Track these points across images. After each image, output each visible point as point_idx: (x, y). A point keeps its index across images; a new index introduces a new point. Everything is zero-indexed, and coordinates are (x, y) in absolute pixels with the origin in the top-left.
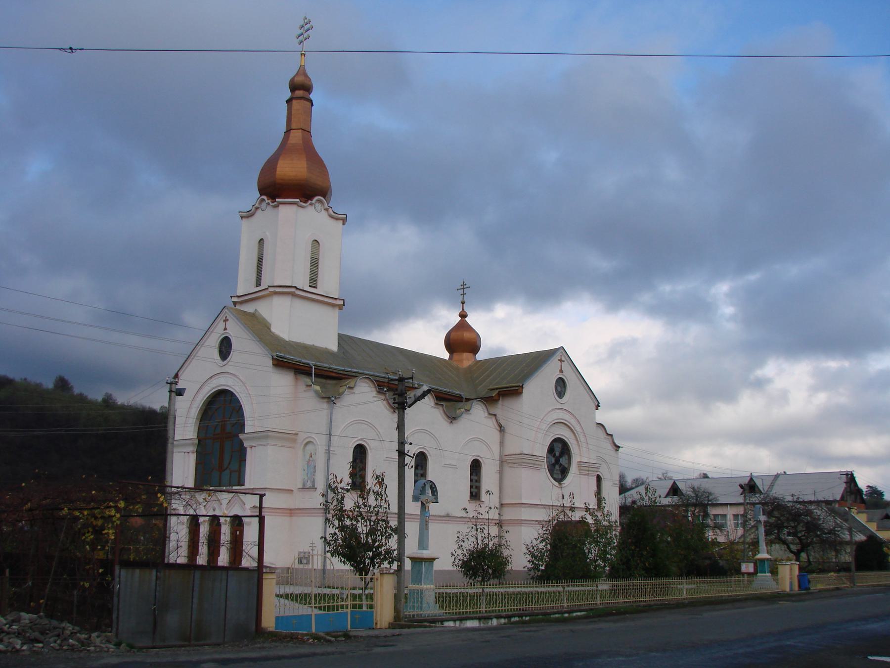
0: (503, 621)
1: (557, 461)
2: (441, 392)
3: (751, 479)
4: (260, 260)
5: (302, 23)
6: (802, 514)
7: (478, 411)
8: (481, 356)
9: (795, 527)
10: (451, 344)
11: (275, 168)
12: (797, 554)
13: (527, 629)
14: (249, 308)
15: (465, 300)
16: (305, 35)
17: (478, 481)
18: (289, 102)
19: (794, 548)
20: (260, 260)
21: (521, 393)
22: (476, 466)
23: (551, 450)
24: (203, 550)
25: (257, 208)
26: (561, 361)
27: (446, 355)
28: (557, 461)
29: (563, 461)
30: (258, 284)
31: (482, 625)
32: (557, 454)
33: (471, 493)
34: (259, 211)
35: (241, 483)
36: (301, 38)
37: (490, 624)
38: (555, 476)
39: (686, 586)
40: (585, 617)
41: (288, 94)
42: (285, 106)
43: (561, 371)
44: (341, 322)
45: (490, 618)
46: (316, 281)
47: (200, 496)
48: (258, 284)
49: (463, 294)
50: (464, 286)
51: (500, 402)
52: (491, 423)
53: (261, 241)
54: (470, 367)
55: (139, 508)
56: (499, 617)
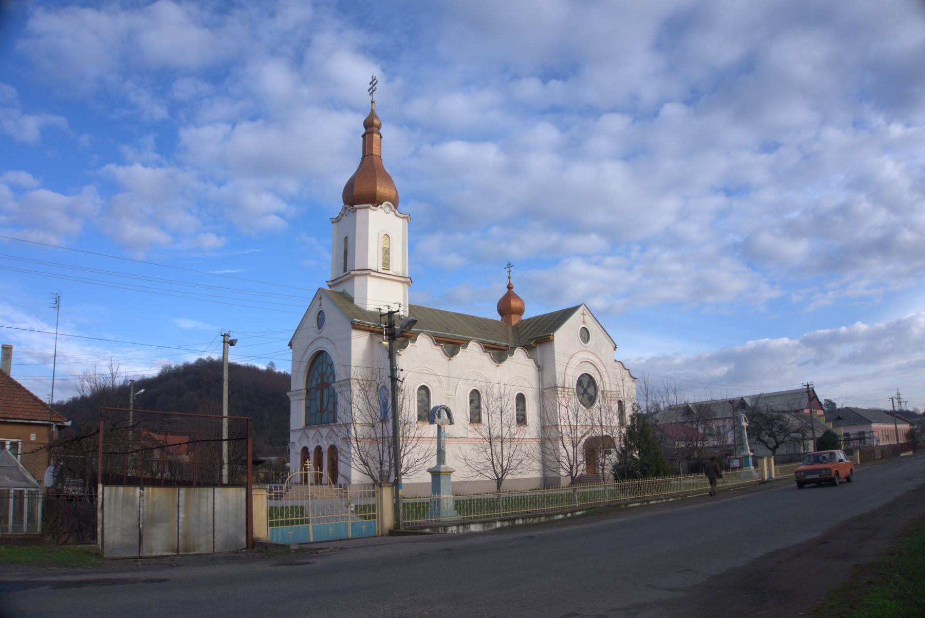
0: (506, 524)
1: (585, 391)
2: (487, 343)
4: (346, 252)
6: (774, 420)
7: (519, 354)
8: (525, 317)
9: (771, 430)
12: (773, 450)
15: (505, 273)
17: (524, 409)
18: (364, 136)
19: (771, 446)
20: (346, 252)
21: (553, 340)
22: (521, 398)
23: (579, 383)
24: (113, 493)
26: (583, 314)
28: (585, 391)
29: (591, 391)
30: (345, 270)
31: (486, 529)
33: (518, 420)
35: (335, 421)
37: (494, 527)
39: (683, 482)
41: (363, 131)
42: (362, 139)
43: (584, 322)
45: (541, 516)
47: (311, 433)
48: (345, 270)
50: (509, 265)
52: (531, 363)
53: (346, 237)
54: (516, 325)
55: (157, 454)
56: (502, 520)
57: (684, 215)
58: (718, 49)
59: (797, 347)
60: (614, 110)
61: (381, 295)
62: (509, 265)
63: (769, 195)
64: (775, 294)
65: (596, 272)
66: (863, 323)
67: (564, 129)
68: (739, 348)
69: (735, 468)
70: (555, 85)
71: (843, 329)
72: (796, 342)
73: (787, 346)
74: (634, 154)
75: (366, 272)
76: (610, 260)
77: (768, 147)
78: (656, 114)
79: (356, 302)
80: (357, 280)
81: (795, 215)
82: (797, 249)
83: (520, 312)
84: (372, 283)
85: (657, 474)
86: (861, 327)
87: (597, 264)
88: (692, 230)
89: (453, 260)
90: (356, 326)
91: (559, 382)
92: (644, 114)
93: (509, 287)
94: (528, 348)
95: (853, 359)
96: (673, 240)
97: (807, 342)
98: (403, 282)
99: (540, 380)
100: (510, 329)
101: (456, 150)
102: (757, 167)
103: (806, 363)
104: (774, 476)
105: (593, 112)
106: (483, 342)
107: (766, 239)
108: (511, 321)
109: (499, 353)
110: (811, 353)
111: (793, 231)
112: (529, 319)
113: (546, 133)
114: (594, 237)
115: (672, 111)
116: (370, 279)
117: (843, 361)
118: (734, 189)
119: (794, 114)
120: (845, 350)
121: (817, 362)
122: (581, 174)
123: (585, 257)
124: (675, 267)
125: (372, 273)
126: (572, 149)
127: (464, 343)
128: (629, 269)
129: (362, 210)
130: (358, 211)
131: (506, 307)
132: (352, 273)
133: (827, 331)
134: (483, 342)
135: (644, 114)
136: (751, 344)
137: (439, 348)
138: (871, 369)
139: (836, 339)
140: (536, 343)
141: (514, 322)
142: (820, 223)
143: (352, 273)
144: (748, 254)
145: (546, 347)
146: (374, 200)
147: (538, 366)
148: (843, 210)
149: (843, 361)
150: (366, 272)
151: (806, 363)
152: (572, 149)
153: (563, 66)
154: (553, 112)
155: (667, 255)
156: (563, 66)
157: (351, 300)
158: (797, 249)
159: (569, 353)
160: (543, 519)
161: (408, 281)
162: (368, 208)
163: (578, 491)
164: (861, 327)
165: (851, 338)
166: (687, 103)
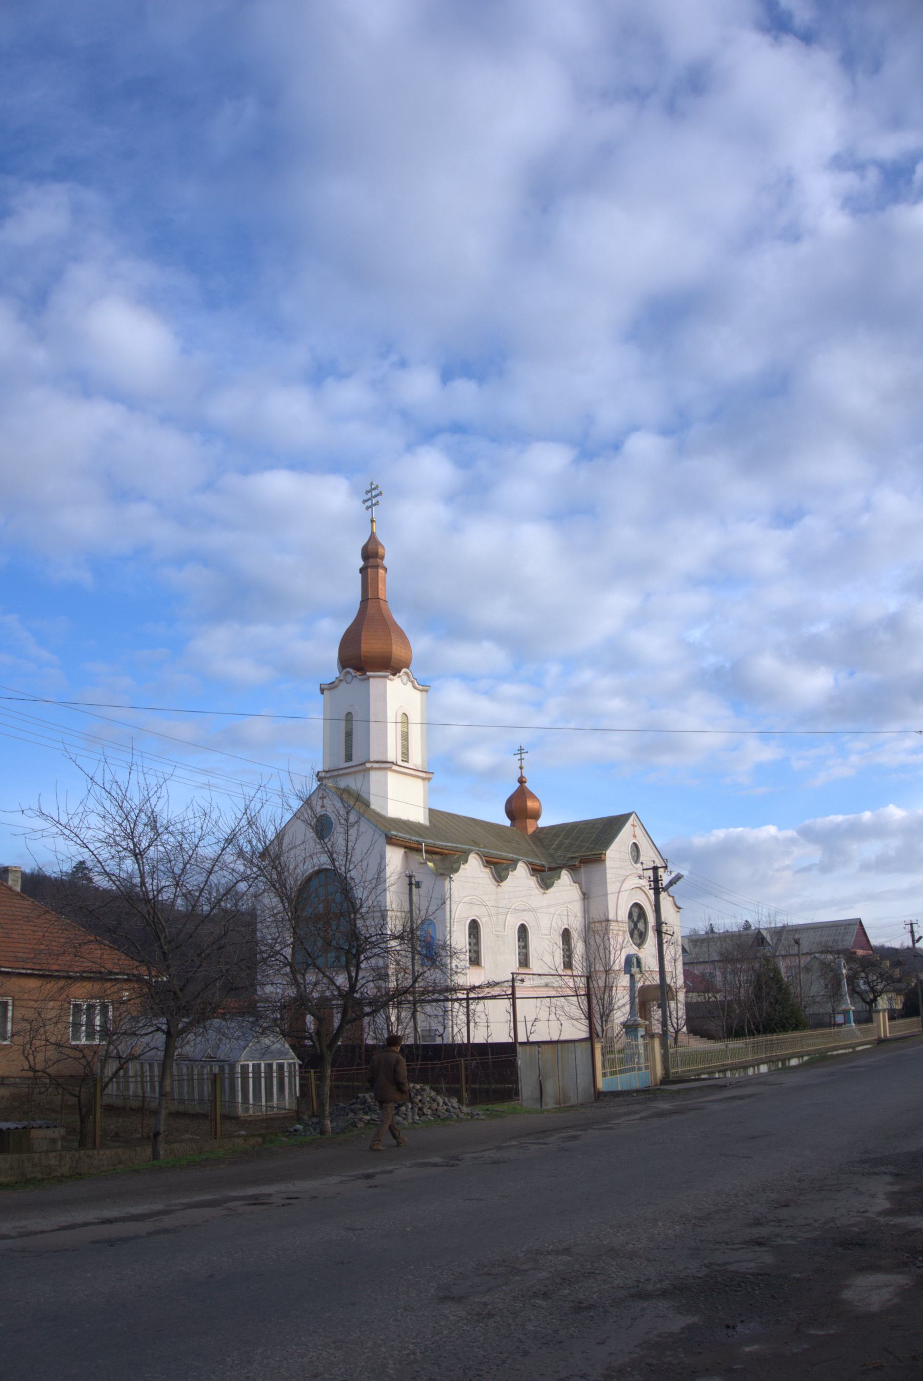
3: (759, 932)
4: (349, 735)
5: (369, 488)
10: (511, 812)
11: (358, 642)
13: (710, 1098)
14: (343, 783)
15: (523, 765)
16: (374, 501)
18: (363, 570)
20: (349, 735)
21: (604, 860)
23: (630, 915)
25: (341, 681)
26: (633, 826)
27: (507, 822)
29: (641, 925)
30: (349, 757)
32: (635, 919)
34: (344, 683)
36: (369, 504)
38: (315, 882)
40: (125, 980)
41: (361, 563)
42: (360, 575)
43: (634, 836)
44: (430, 793)
46: (407, 755)
48: (349, 757)
49: (521, 759)
50: (521, 749)
51: (582, 870)
54: (534, 832)
57: (640, 619)
58: (730, 353)
59: (793, 841)
60: (550, 437)
61: (403, 799)
62: (521, 749)
63: (781, 596)
64: (767, 754)
65: (485, 707)
66: (899, 806)
67: (463, 461)
68: (698, 841)
69: (840, 1025)
70: (465, 388)
71: (867, 816)
72: (790, 833)
73: (775, 840)
74: (572, 513)
75: (385, 765)
76: (508, 689)
77: (785, 518)
78: (616, 447)
79: (372, 807)
80: (374, 776)
81: (821, 628)
82: (814, 684)
83: (536, 816)
84: (392, 778)
85: (796, 1028)
86: (895, 813)
87: (489, 694)
88: (652, 644)
89: (245, 670)
90: (391, 841)
91: (611, 916)
92: (595, 448)
93: (521, 781)
94: (573, 869)
95: (882, 865)
96: (617, 658)
97: (809, 834)
98: (423, 779)
99: (586, 911)
100: (528, 839)
101: (278, 485)
102: (767, 550)
103: (807, 869)
104: (888, 1035)
105: (516, 436)
106: (531, 864)
107: (767, 665)
108: (525, 828)
109: (545, 875)
110: (813, 853)
111: (811, 652)
112: (552, 828)
113: (433, 467)
114: (487, 645)
115: (644, 446)
116: (390, 775)
117: (867, 867)
118: (722, 576)
119: (835, 465)
120: (871, 849)
121: (825, 868)
122: (481, 540)
123: (468, 678)
124: (616, 704)
125: (394, 767)
126: (473, 495)
127: (513, 864)
128: (539, 706)
129: (378, 680)
130: (371, 680)
131: (519, 807)
132: (368, 765)
133: (840, 818)
134: (531, 864)
135: (595, 448)
136: (720, 834)
137: (488, 870)
138: (904, 881)
139: (857, 832)
140: (581, 862)
141: (531, 830)
142: (854, 645)
143: (368, 765)
144: (732, 684)
145: (594, 868)
146: (390, 665)
147: (584, 894)
148: (894, 624)
149: (867, 867)
150: (385, 765)
151: (807, 869)
152: (473, 495)
153: (478, 359)
154: (449, 433)
155: (606, 682)
156: (478, 359)
157: (367, 804)
158: (814, 684)
159: (622, 881)
160: (806, 1058)
161: (426, 775)
162: (386, 677)
163: (730, 1046)
164: (895, 813)
165: (878, 830)
166: (665, 431)
